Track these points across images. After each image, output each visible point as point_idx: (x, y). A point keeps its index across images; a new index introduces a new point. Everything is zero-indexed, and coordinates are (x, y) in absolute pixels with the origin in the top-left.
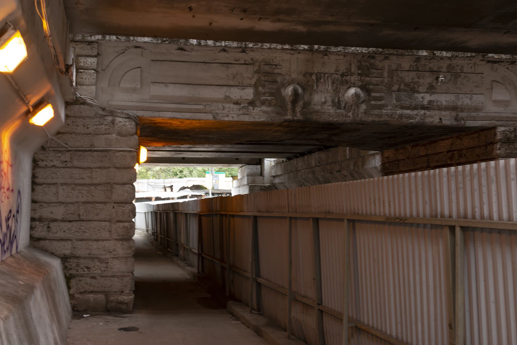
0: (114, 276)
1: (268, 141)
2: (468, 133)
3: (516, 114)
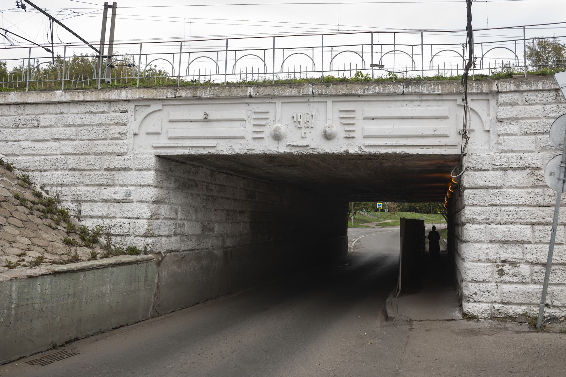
0: (527, 223)
3: (474, 4)
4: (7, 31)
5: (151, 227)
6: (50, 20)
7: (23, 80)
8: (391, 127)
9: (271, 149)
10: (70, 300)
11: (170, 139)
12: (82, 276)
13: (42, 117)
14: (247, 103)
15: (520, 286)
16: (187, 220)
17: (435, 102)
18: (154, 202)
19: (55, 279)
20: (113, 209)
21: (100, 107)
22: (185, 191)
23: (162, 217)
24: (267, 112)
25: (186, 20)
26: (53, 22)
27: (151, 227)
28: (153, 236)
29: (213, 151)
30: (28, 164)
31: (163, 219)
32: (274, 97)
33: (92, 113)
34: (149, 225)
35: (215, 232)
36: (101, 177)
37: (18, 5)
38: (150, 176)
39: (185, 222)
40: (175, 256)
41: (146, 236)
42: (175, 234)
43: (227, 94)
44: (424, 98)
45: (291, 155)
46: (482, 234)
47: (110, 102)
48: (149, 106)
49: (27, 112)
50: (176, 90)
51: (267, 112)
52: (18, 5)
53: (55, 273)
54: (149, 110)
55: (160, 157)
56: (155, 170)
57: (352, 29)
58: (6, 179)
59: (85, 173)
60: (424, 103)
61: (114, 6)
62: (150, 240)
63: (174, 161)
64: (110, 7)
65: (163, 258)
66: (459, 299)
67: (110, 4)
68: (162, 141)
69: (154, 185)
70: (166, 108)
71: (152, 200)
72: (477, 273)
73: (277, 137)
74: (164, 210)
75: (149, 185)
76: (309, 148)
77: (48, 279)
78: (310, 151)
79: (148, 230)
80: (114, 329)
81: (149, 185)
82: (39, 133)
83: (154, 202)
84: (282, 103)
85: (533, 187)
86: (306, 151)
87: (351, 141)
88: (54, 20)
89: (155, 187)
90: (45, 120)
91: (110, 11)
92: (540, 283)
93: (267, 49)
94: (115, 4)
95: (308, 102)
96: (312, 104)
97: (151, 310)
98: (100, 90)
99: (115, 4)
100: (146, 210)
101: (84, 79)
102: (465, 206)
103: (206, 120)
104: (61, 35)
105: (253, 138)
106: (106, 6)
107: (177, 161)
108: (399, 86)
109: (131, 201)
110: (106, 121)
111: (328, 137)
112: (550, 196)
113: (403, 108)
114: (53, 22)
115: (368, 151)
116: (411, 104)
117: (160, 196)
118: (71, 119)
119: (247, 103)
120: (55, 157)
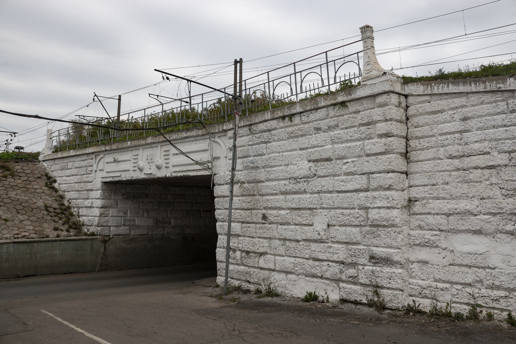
2: (60, 320)
4: (158, 96)
5: (100, 221)
6: (188, 82)
7: (98, 139)
8: (183, 159)
9: (139, 176)
10: (28, 256)
11: (107, 172)
12: (36, 245)
13: (69, 164)
14: (131, 150)
15: (236, 267)
16: (137, 217)
17: (203, 140)
18: (101, 208)
19: (16, 246)
20: (88, 212)
21: (85, 157)
22: (135, 200)
23: (110, 216)
24: (169, 151)
25: (259, 69)
26: (190, 83)
27: (100, 221)
28: (102, 226)
29: (120, 179)
30: (64, 189)
31: (112, 216)
32: (139, 146)
33: (83, 160)
34: (99, 220)
35: (172, 225)
36: (84, 194)
37: (163, 78)
38: (98, 194)
39: (136, 218)
40: (122, 238)
41: (98, 226)
42: (124, 225)
43: (144, 143)
44: (197, 139)
45: (145, 178)
46: (221, 229)
47: (88, 154)
48: (99, 155)
49: (65, 162)
50: (105, 146)
51: (169, 151)
52: (163, 78)
53: (15, 242)
54: (99, 157)
55: (105, 183)
56: (102, 190)
58: (47, 197)
59: (81, 192)
60: (198, 142)
61: (241, 61)
62: (99, 229)
63: (122, 184)
64: (238, 62)
65: (110, 239)
66: (213, 272)
67: (238, 60)
68: (105, 175)
69: (101, 198)
70: (106, 156)
71: (100, 206)
72: (219, 255)
73: (141, 170)
74: (111, 212)
75: (98, 199)
76: (152, 175)
77: (12, 245)
78: (153, 176)
79: (98, 223)
80: (64, 274)
81: (98, 199)
82: (68, 172)
83: (101, 208)
84: (143, 149)
85: (243, 196)
86: (152, 177)
87: (168, 169)
88: (191, 81)
89: (103, 199)
90: (70, 165)
91: (238, 65)
92: (227, 197)
93: (148, 108)
94: (241, 59)
95: (151, 147)
96: (154, 148)
97: (98, 267)
98: (88, 147)
99: (241, 59)
100: (97, 212)
101: (211, 116)
102: (214, 185)
103: (115, 161)
104: (196, 89)
105: (133, 170)
106: (236, 62)
107: (122, 184)
108: (183, 133)
109: (93, 207)
110: (87, 164)
111: (159, 168)
112: (249, 202)
113: (188, 146)
114: (190, 83)
115: (174, 175)
116: (193, 143)
117: (106, 204)
118: (77, 164)
119: (131, 150)
120: (72, 184)
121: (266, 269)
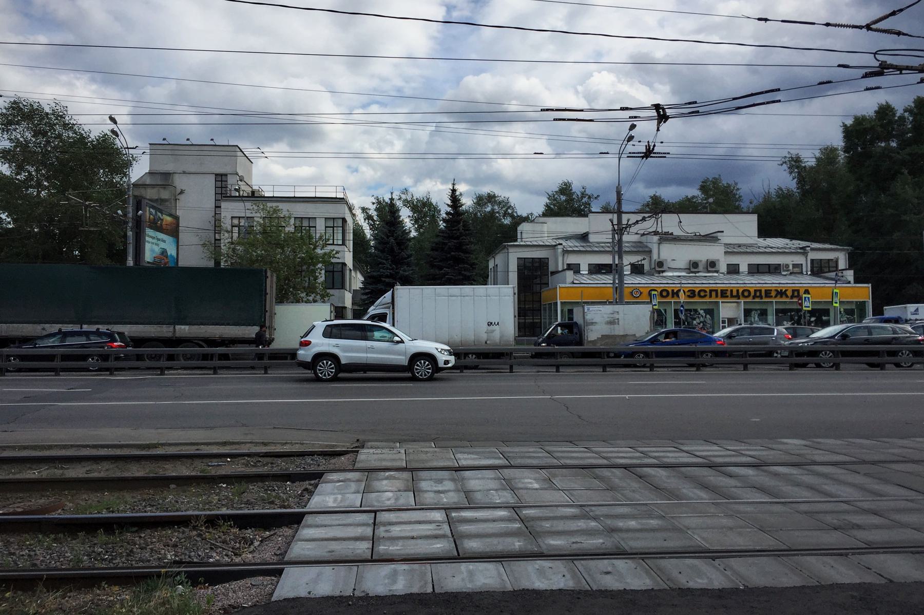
1: (25, 448)
57: (568, 107)
121: (848, 513)
